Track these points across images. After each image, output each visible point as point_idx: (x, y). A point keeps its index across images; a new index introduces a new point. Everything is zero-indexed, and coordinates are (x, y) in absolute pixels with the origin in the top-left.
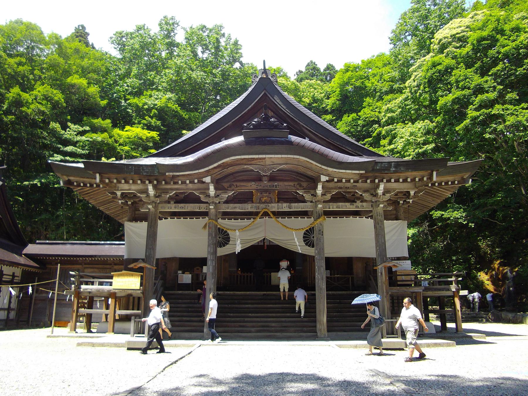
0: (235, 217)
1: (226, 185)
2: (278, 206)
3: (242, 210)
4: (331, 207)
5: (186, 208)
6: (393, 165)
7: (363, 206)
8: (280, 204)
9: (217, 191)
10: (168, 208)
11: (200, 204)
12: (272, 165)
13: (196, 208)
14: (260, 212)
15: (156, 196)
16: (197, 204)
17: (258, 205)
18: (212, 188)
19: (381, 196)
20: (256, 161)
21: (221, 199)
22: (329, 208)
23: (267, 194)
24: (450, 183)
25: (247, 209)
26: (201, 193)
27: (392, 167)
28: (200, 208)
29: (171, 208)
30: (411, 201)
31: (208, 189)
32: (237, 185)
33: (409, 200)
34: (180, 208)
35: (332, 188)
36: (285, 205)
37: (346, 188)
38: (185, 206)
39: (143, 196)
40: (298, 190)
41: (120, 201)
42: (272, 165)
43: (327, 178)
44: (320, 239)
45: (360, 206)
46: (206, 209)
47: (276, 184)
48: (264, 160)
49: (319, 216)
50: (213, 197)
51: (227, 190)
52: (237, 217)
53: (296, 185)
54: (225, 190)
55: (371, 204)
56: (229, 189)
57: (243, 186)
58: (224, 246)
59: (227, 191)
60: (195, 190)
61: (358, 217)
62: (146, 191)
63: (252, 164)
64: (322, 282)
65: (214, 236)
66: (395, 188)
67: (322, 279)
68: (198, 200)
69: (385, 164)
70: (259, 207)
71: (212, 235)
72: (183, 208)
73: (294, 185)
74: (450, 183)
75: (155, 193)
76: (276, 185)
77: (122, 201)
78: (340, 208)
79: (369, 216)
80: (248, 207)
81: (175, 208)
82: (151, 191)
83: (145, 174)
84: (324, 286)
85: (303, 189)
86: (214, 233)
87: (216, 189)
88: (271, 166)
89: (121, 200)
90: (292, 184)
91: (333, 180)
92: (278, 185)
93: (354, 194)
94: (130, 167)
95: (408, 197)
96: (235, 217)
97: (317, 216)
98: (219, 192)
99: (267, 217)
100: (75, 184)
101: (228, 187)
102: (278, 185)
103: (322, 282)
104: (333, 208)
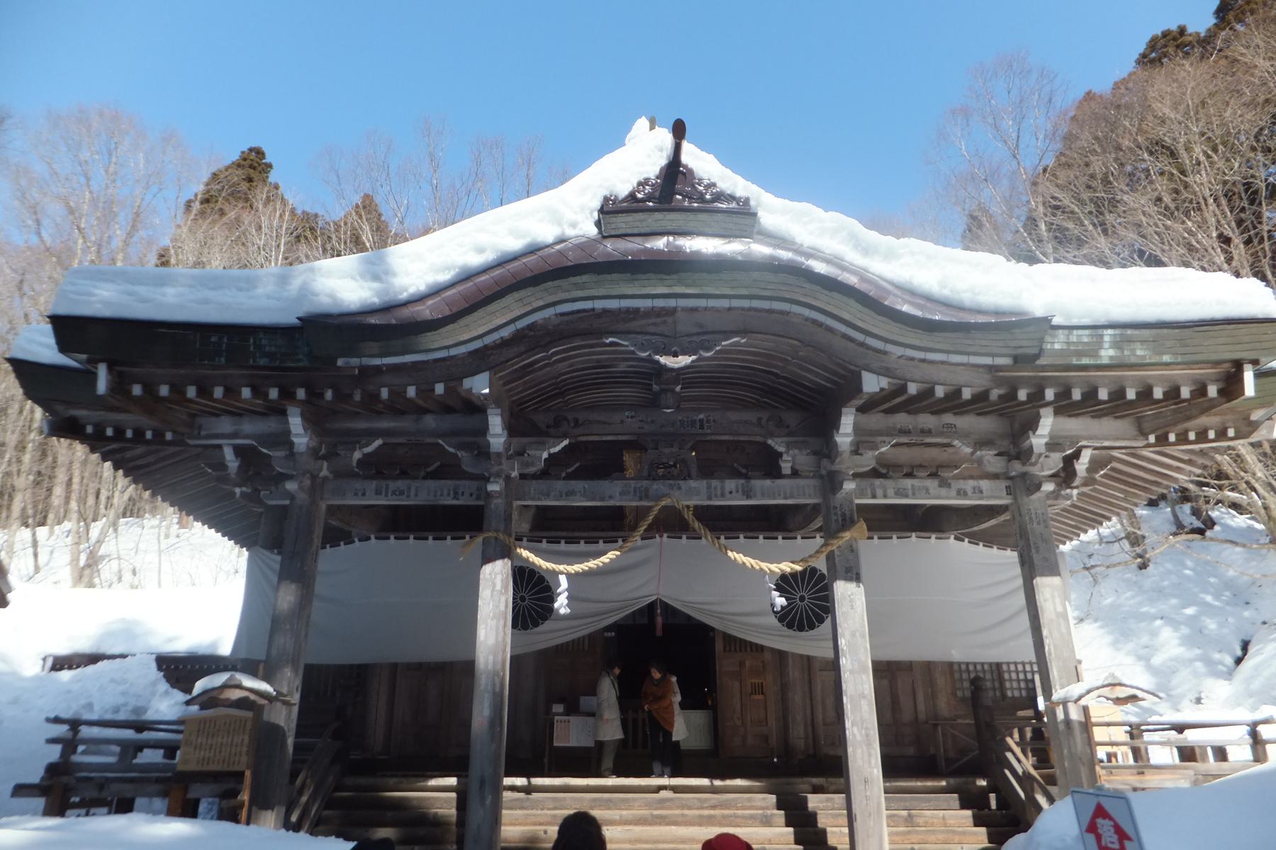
0: (570, 534)
1: (542, 419)
2: (709, 487)
3: (593, 500)
4: (879, 492)
5: (412, 493)
6: (1107, 339)
7: (981, 492)
8: (715, 483)
9: (515, 440)
10: (356, 494)
11: (458, 482)
12: (698, 334)
13: (446, 492)
14: (649, 509)
15: (314, 453)
16: (449, 482)
17: (645, 483)
18: (496, 423)
19: (1040, 455)
20: (643, 322)
21: (527, 465)
22: (874, 497)
23: (674, 450)
24: (1212, 434)
25: (611, 497)
26: (461, 447)
27: (1106, 345)
28: (456, 493)
29: (364, 494)
30: (1075, 492)
31: (484, 430)
32: (576, 421)
33: (1068, 491)
34: (394, 493)
35: (879, 433)
36: (731, 484)
37: (922, 431)
38: (409, 488)
39: (277, 454)
40: (772, 435)
41: (238, 490)
42: (698, 334)
43: (884, 382)
44: (851, 601)
45: (969, 491)
46: (478, 498)
47: (701, 416)
48: (670, 320)
49: (844, 520)
50: (498, 455)
51: (548, 435)
52: (576, 534)
53: (764, 421)
54: (541, 434)
55: (1008, 483)
56: (552, 431)
57: (598, 422)
58: (536, 625)
59: (546, 439)
60: (443, 435)
61: (933, 536)
62: (283, 439)
63: (629, 332)
64: (870, 755)
65: (498, 587)
66: (1074, 433)
67: (869, 745)
68: (450, 470)
69: (1080, 332)
70: (647, 490)
71: (494, 585)
72: (402, 493)
73: (760, 419)
74: (1212, 434)
75: (313, 444)
76: (701, 421)
77: (244, 489)
78: (906, 496)
79: (967, 535)
80: (612, 494)
81: (378, 492)
82: (298, 435)
83: (263, 362)
84: (877, 772)
85: (788, 435)
86: (499, 578)
87: (513, 430)
88: (695, 338)
89: (240, 486)
90: (751, 416)
91: (902, 389)
92: (708, 421)
93: (910, 471)
94: (214, 339)
95: (1065, 482)
96: (570, 534)
97: (837, 521)
98: (518, 442)
99: (665, 535)
100: (89, 429)
101: (548, 427)
102: (708, 421)
103: (870, 755)
104: (885, 496)
